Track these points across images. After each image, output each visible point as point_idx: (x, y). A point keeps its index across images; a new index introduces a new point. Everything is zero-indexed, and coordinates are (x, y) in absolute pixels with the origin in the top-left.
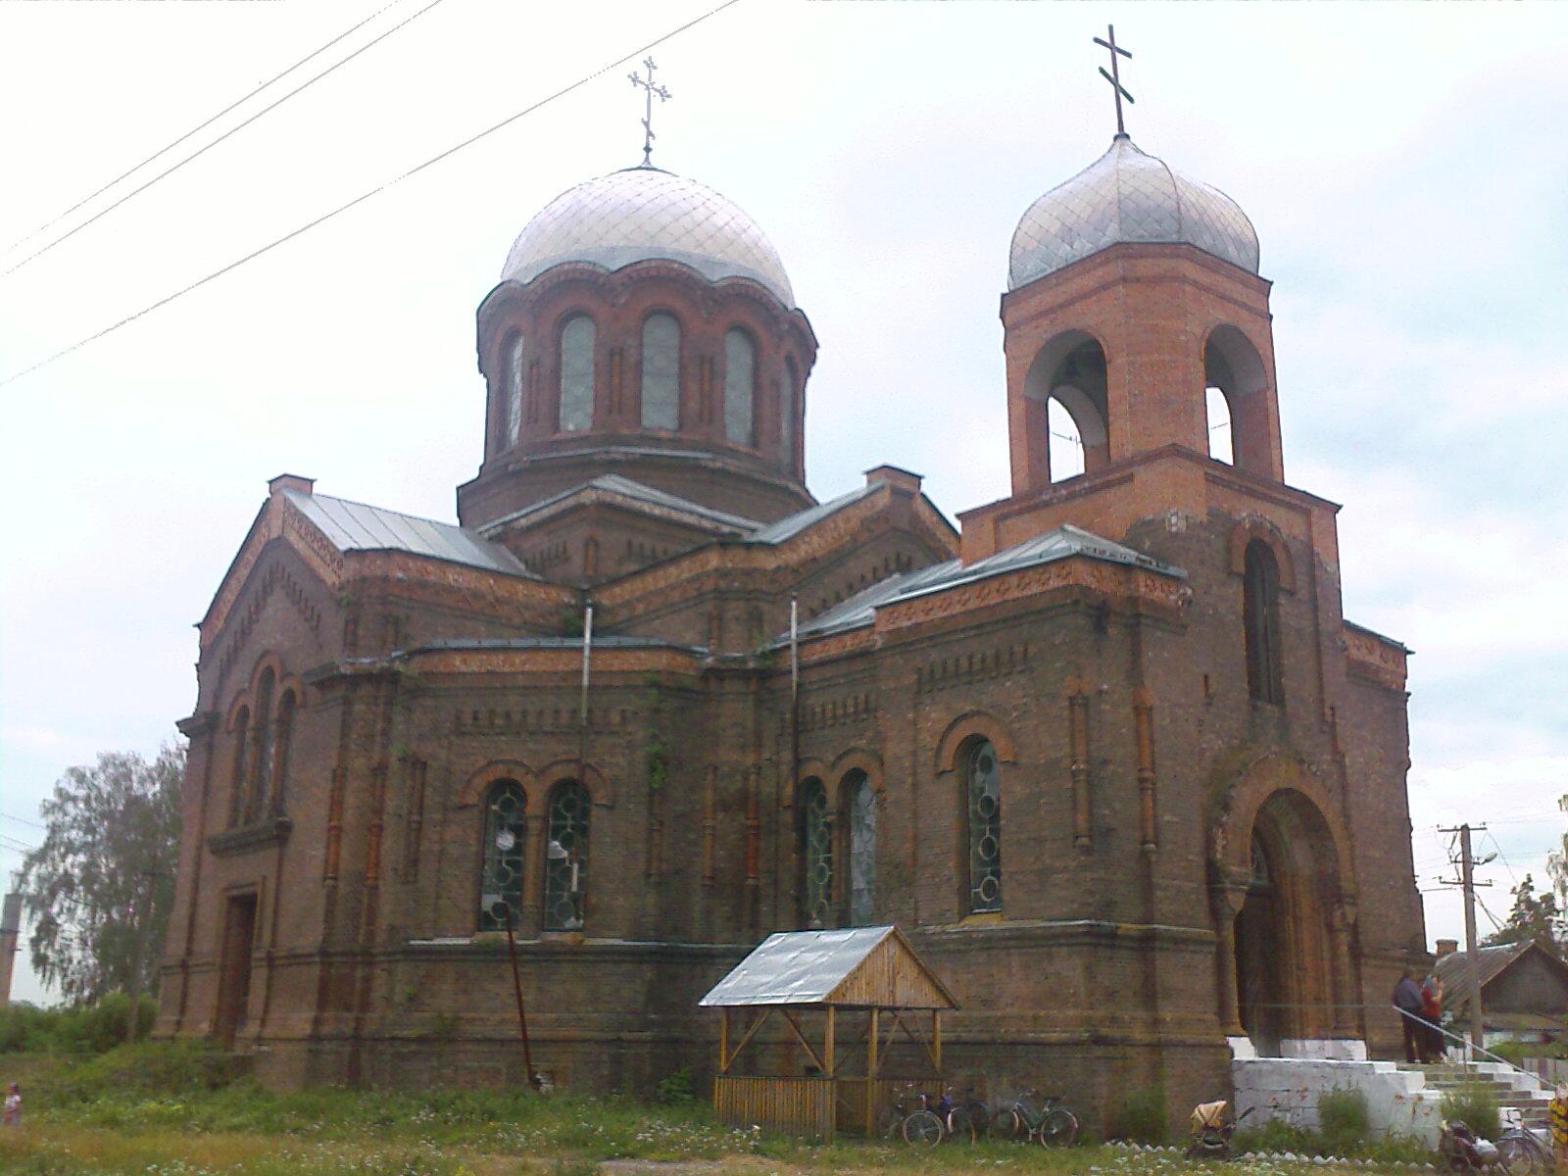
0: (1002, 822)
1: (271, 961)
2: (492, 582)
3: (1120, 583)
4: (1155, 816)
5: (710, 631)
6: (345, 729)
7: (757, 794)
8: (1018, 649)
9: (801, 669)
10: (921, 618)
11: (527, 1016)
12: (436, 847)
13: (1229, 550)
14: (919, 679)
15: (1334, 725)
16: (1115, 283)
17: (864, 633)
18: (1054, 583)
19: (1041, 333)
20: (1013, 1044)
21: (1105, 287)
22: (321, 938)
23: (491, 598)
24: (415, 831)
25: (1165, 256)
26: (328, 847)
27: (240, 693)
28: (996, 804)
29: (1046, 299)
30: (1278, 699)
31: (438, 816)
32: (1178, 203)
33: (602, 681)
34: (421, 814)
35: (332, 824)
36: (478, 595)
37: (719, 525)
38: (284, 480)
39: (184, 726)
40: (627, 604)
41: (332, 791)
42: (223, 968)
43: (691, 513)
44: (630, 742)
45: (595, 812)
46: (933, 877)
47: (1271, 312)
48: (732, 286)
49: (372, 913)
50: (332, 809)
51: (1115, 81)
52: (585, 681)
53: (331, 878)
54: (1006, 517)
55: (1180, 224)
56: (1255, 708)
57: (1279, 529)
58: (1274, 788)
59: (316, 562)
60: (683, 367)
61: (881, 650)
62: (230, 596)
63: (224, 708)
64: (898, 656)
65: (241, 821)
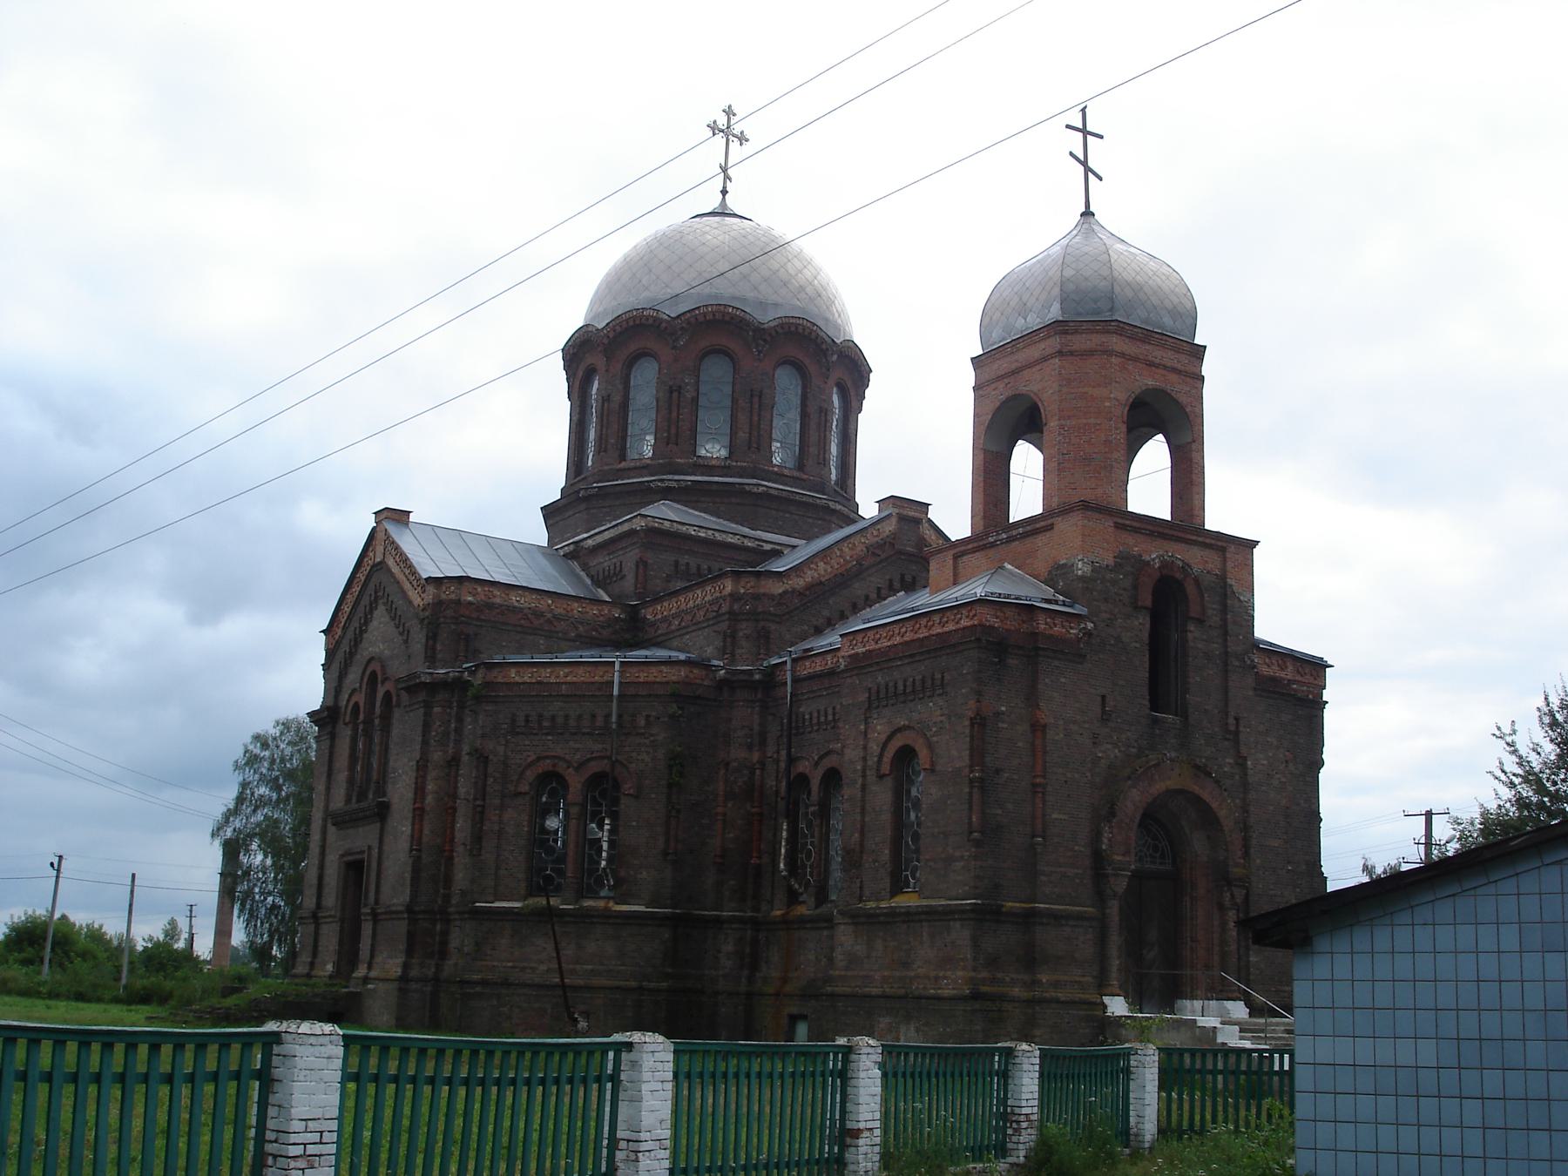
1: (375, 916)
2: (550, 602)
3: (1024, 622)
4: (1044, 815)
5: (724, 647)
6: (426, 727)
9: (795, 681)
10: (872, 646)
12: (496, 828)
14: (869, 698)
15: (1237, 733)
16: (1052, 356)
18: (965, 623)
19: (1000, 393)
20: (920, 998)
21: (1045, 359)
22: (408, 899)
23: (549, 615)
24: (479, 815)
26: (413, 824)
27: (354, 691)
32: (1112, 285)
33: (632, 691)
34: (484, 800)
35: (417, 805)
36: (538, 614)
38: (385, 511)
40: (665, 619)
41: (416, 778)
42: (342, 920)
44: (653, 741)
45: (624, 800)
47: (1203, 374)
48: (782, 325)
49: (448, 881)
50: (416, 794)
51: (1084, 163)
52: (616, 692)
53: (416, 850)
54: (963, 553)
55: (1113, 302)
57: (1189, 566)
59: (407, 586)
60: (734, 401)
61: (843, 671)
64: (854, 677)
65: (354, 800)
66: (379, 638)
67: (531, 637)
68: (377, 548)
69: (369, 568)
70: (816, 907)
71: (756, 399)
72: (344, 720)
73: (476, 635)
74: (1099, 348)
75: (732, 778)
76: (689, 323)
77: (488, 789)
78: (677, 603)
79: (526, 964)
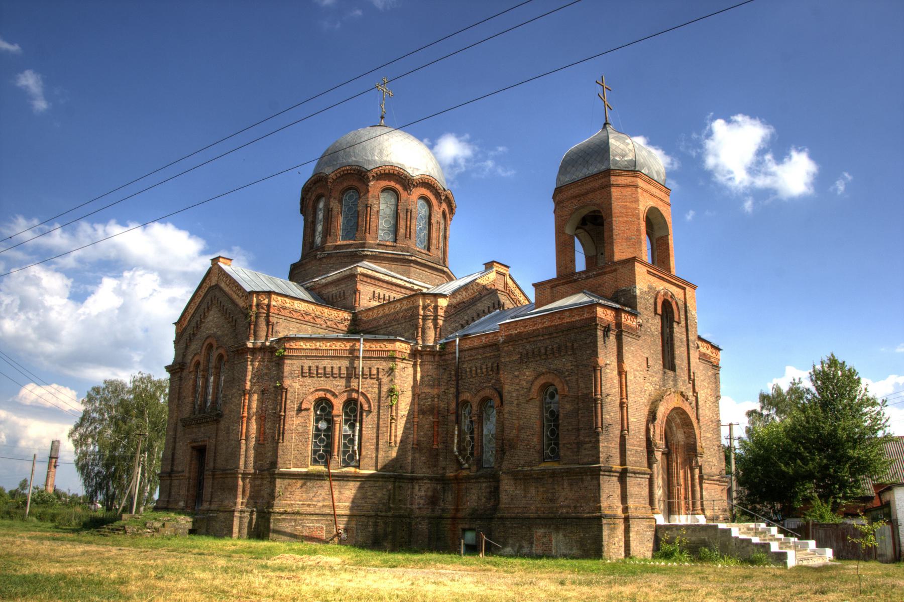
0: (560, 421)
8: (569, 344)
10: (522, 329)
11: (335, 504)
13: (655, 304)
15: (694, 381)
20: (565, 518)
25: (629, 176)
28: (556, 413)
30: (673, 368)
37: (413, 285)
39: (169, 369)
43: (401, 280)
46: (527, 446)
52: (457, 355)
56: (665, 372)
58: (673, 407)
59: (235, 296)
67: (305, 326)
68: (213, 278)
69: (206, 289)
70: (477, 471)
71: (409, 214)
73: (277, 323)
74: (631, 184)
75: (422, 403)
78: (383, 310)
79: (310, 503)
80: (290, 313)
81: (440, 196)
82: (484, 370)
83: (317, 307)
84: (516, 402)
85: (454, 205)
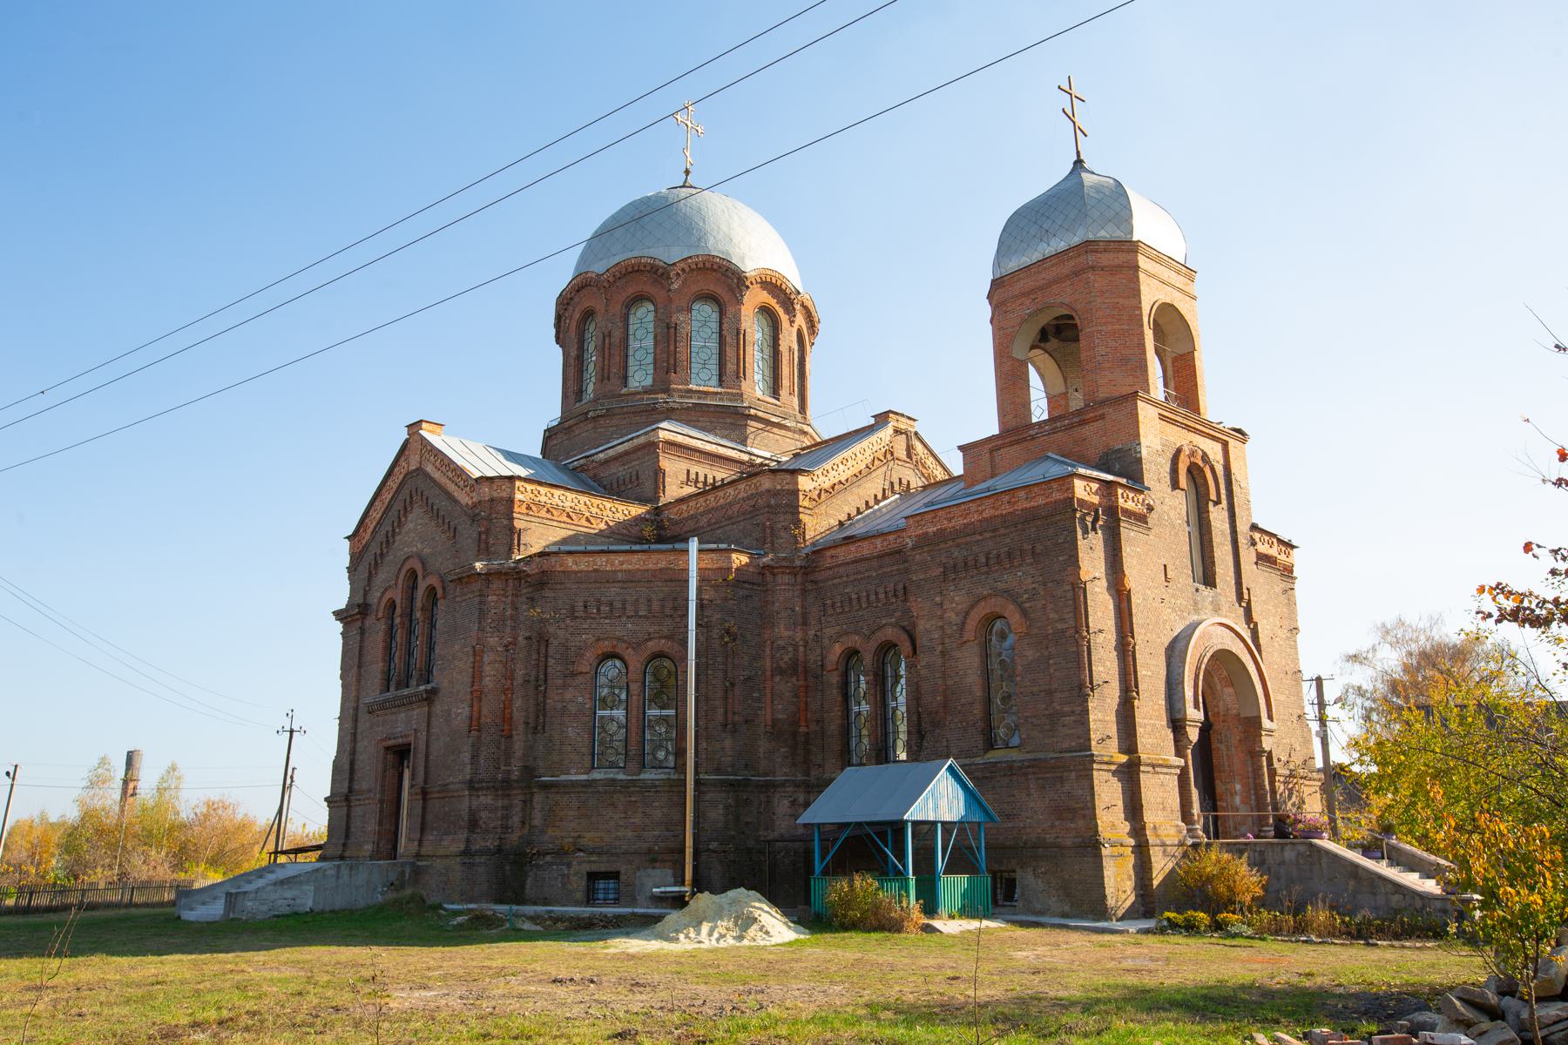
7: (806, 662)
8: (1027, 547)
17: (892, 537)
26: (472, 706)
29: (1027, 283)
31: (559, 682)
54: (999, 448)
59: (451, 487)
62: (376, 515)
63: (374, 598)
66: (417, 539)
69: (401, 477)
72: (377, 615)
76: (683, 270)
77: (549, 670)
80: (548, 511)
81: (792, 304)
82: (882, 596)
83: (593, 501)
84: (940, 648)
85: (816, 319)
